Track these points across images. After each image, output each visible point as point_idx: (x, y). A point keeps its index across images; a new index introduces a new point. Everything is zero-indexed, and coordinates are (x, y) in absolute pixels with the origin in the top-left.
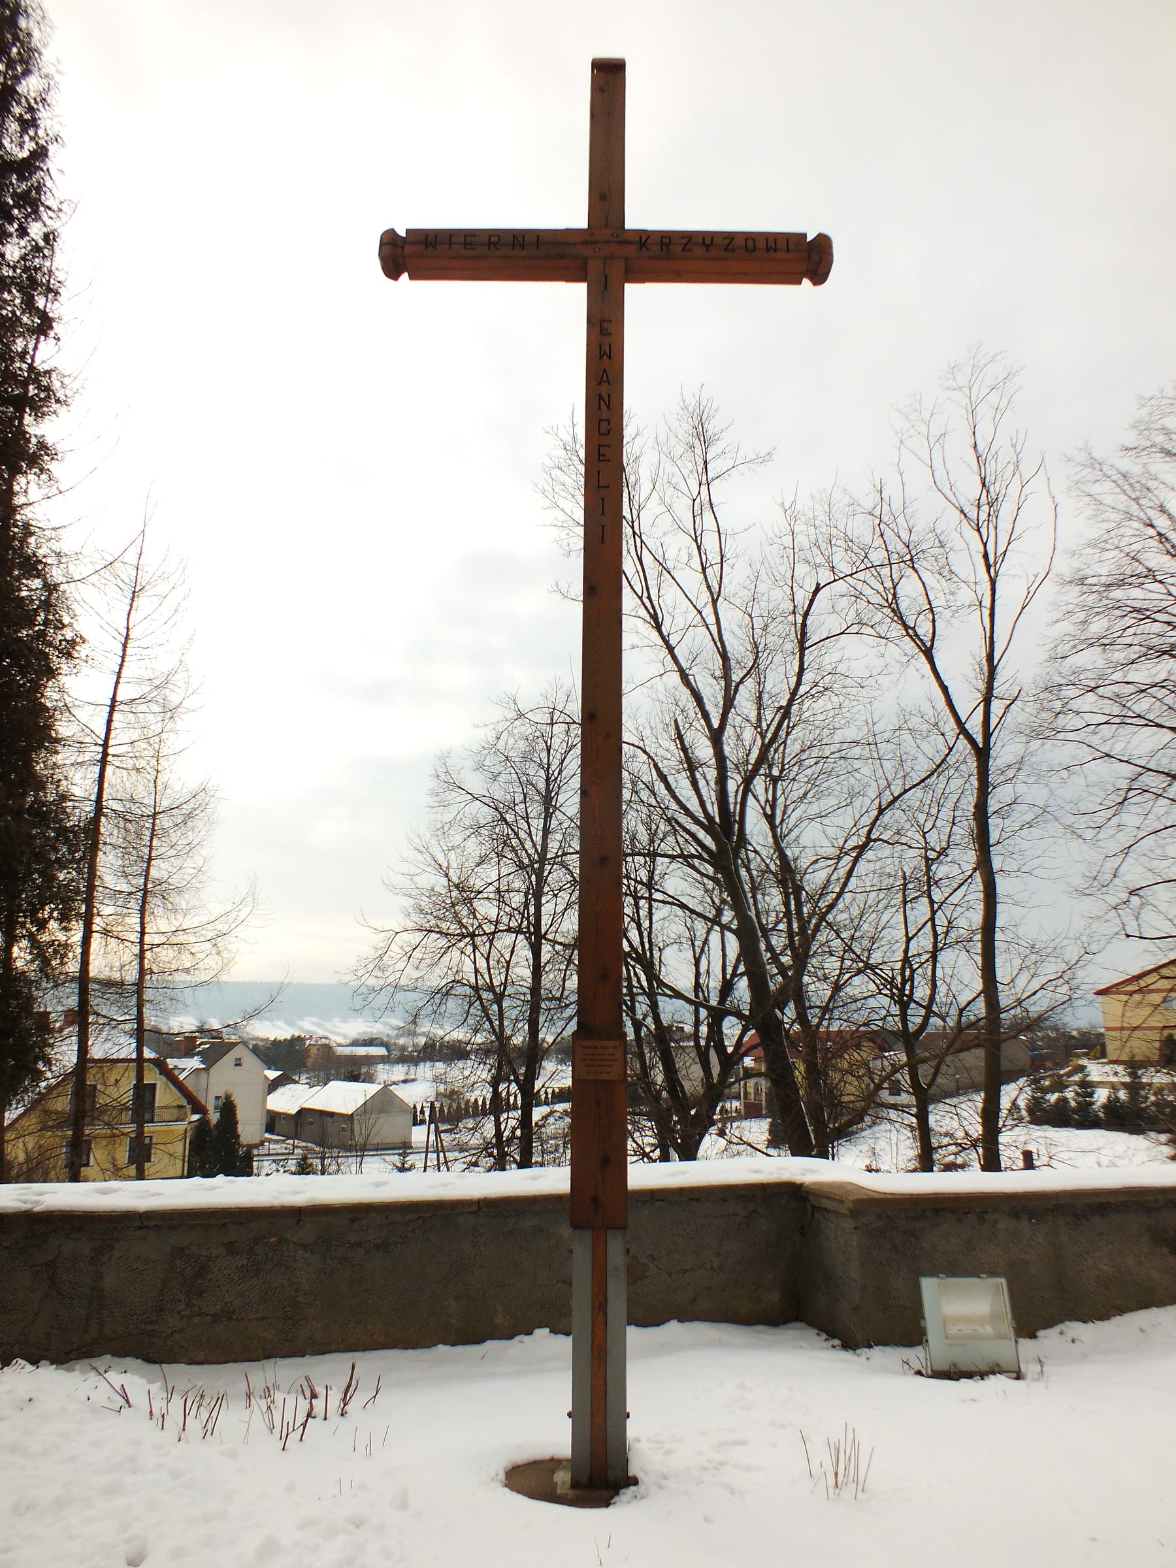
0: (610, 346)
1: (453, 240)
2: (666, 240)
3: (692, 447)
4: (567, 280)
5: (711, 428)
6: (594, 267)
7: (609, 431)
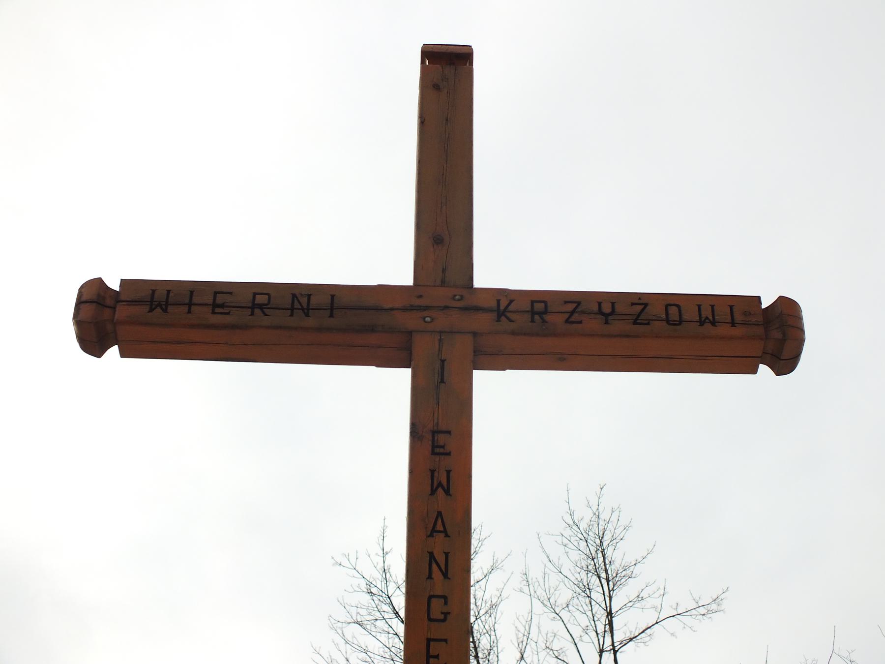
0: (448, 472)
1: (195, 300)
2: (539, 307)
3: (587, 590)
4: (378, 366)
5: (618, 557)
6: (423, 345)
7: (446, 614)
